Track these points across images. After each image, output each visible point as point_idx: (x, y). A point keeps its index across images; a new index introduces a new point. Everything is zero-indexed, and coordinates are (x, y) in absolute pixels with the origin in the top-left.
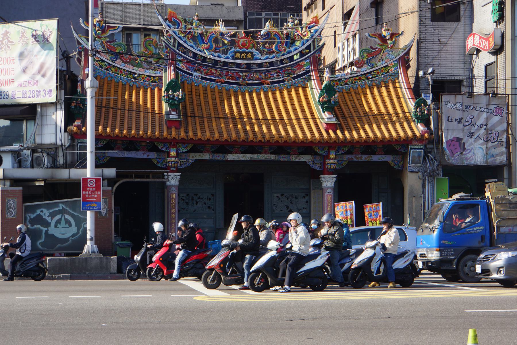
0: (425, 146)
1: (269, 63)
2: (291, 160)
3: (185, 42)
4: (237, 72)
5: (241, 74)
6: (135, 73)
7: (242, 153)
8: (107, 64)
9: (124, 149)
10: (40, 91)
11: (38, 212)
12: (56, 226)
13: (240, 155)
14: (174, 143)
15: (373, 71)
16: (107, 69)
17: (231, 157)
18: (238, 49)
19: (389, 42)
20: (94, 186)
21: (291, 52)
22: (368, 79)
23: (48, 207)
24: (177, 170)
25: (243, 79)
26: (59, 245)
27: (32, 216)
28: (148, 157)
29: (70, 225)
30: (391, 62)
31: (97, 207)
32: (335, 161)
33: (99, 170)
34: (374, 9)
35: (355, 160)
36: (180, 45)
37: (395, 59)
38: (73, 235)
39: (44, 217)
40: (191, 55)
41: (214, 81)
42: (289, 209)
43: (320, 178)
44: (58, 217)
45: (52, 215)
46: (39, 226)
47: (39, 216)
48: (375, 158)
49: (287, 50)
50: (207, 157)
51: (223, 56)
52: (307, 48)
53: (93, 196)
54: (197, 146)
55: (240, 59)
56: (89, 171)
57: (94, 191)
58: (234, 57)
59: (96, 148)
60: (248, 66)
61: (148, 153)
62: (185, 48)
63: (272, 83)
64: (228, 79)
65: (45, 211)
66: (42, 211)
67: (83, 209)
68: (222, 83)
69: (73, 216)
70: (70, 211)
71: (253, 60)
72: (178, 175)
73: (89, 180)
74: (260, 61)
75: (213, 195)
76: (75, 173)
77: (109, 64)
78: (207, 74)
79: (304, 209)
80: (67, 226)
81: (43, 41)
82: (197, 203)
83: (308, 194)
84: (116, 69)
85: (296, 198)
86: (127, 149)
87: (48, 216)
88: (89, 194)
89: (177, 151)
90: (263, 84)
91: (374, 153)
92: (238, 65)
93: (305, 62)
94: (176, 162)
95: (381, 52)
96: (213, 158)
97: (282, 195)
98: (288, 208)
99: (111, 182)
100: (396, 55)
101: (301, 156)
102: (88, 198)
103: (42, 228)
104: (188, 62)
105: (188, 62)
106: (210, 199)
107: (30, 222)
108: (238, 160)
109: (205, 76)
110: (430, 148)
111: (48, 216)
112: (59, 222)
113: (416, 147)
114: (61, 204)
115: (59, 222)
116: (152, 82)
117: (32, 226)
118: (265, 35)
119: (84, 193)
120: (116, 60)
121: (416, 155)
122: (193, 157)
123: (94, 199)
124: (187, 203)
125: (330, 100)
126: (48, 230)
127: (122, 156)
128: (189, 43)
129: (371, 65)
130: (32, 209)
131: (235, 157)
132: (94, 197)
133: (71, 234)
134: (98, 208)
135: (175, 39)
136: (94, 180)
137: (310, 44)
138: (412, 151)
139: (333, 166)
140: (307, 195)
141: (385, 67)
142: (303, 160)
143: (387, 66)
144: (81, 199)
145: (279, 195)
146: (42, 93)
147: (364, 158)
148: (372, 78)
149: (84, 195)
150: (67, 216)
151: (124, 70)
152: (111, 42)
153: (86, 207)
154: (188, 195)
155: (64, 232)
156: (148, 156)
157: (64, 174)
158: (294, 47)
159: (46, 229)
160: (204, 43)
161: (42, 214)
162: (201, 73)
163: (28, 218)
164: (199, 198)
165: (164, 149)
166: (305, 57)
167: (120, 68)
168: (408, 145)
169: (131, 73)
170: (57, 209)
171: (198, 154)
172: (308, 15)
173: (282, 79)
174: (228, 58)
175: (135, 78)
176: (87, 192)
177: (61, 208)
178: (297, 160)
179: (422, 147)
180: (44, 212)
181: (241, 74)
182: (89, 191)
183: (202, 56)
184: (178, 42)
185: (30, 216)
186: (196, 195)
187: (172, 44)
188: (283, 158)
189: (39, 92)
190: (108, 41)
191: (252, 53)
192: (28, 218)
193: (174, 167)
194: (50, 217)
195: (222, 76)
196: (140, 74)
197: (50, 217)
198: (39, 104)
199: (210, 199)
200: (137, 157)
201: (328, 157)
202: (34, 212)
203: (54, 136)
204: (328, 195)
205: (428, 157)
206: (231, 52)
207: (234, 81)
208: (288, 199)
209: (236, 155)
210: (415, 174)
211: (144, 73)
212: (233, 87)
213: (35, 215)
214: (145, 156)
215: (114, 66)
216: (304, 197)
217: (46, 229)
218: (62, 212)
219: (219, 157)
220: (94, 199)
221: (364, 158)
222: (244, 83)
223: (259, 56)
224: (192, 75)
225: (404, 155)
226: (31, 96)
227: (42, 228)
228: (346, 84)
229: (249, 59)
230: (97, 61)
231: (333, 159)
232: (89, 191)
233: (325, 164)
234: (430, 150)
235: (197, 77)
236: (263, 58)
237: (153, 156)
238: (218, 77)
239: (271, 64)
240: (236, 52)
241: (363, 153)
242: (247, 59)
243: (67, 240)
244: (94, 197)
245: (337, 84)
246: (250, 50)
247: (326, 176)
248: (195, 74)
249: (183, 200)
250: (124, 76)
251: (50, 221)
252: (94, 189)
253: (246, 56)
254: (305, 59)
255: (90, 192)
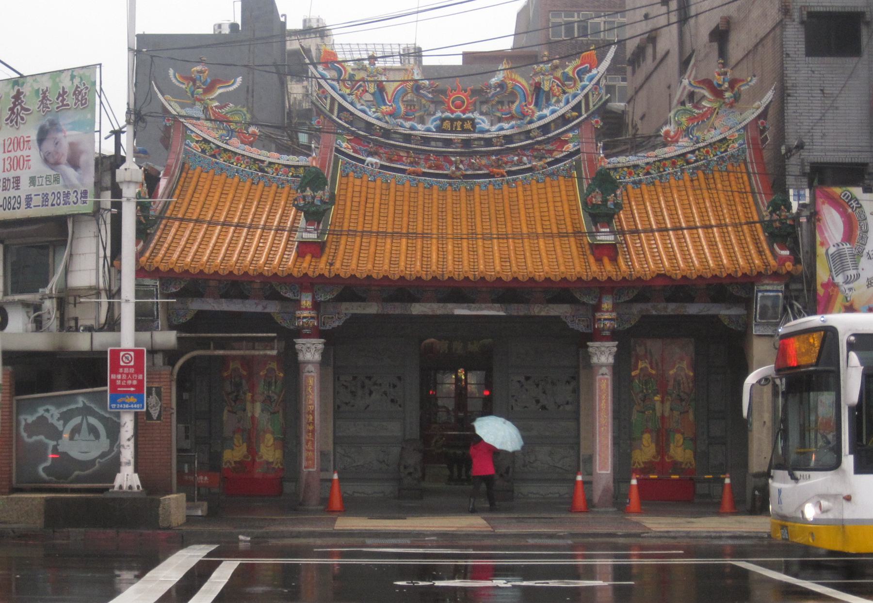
0: (787, 286)
1: (505, 136)
2: (532, 314)
3: (352, 104)
4: (445, 156)
5: (453, 159)
6: (263, 162)
7: (439, 301)
8: (213, 146)
9: (222, 297)
10: (68, 193)
11: (41, 411)
12: (72, 438)
13: (435, 306)
14: (307, 283)
15: (699, 149)
16: (214, 156)
17: (417, 309)
18: (447, 114)
19: (728, 95)
20: (132, 364)
21: (545, 117)
22: (688, 163)
23: (58, 402)
24: (318, 333)
25: (458, 168)
26: (76, 473)
27: (31, 419)
28: (266, 311)
29: (97, 436)
30: (731, 132)
31: (137, 403)
32: (614, 315)
33: (146, 336)
34: (715, 45)
35: (654, 313)
36: (342, 109)
37: (739, 127)
38: (103, 455)
39: (50, 421)
40: (363, 125)
41: (403, 171)
42: (540, 405)
43: (588, 347)
44: (76, 420)
45: (66, 417)
46: (42, 437)
47: (42, 419)
48: (693, 309)
49: (538, 114)
50: (372, 309)
51: (419, 126)
52: (574, 109)
53: (129, 382)
54: (351, 289)
55: (452, 131)
56: (128, 337)
57: (132, 374)
58: (440, 129)
59: (137, 292)
60: (466, 143)
61: (265, 303)
62: (352, 114)
63: (510, 173)
64: (430, 168)
65: (52, 409)
66: (47, 411)
67: (111, 408)
68: (418, 175)
69: (101, 419)
70: (96, 409)
71: (474, 132)
72: (318, 344)
73: (122, 354)
74: (487, 136)
75: (399, 378)
76: (102, 340)
77: (218, 147)
78: (391, 160)
79: (567, 403)
80: (92, 437)
81: (75, 104)
82: (371, 393)
83: (575, 378)
84: (230, 154)
85: (553, 383)
86: (226, 296)
87: (59, 419)
88: (122, 380)
89: (313, 297)
90: (493, 176)
91: (691, 299)
92: (448, 143)
93: (571, 135)
94: (312, 318)
95: (712, 114)
96: (385, 312)
97: (527, 378)
98: (538, 402)
99: (171, 356)
100: (740, 118)
101: (551, 305)
102: (121, 386)
103: (47, 441)
104: (357, 138)
105: (357, 138)
106: (395, 386)
107: (26, 430)
108: (430, 313)
109: (388, 164)
110: (796, 290)
111: (59, 419)
112: (76, 431)
113: (769, 288)
114: (81, 398)
115: (76, 431)
116: (292, 176)
117: (30, 436)
118: (496, 88)
119: (114, 377)
120: (230, 138)
121: (769, 303)
122: (347, 309)
123: (132, 389)
124: (353, 393)
125: (607, 201)
126: (58, 445)
127: (218, 309)
128: (359, 107)
129: (695, 139)
130: (32, 407)
131: (425, 309)
132: (132, 386)
133: (98, 453)
134: (138, 406)
135: (333, 99)
136: (132, 354)
137: (580, 102)
138: (760, 294)
139: (608, 324)
140: (573, 378)
141: (721, 141)
142: (552, 313)
143: (725, 139)
144: (108, 388)
145: (522, 379)
146: (72, 198)
147: (672, 309)
148: (696, 161)
149: (113, 382)
150: (92, 420)
151: (243, 155)
152: (221, 108)
153: (116, 403)
154: (355, 378)
155: (84, 449)
156: (265, 308)
157: (82, 342)
158: (551, 108)
159: (54, 443)
160: (385, 104)
161: (47, 415)
162: (381, 159)
163: (23, 423)
164: (375, 384)
165: (289, 295)
166: (571, 125)
167: (236, 153)
168: (753, 284)
169: (256, 160)
170: (73, 406)
171: (355, 304)
172: (634, 72)
173: (528, 166)
174: (429, 130)
175: (262, 170)
176: (119, 376)
177: (80, 405)
178: (543, 314)
179: (779, 288)
180: (51, 412)
181: (453, 159)
182: (121, 374)
183: (381, 128)
184: (340, 104)
185: (26, 420)
186: (370, 378)
187: (328, 108)
188: (518, 310)
189: (67, 195)
190: (216, 107)
191: (472, 120)
192: (23, 423)
193: (308, 328)
194: (61, 422)
195: (418, 163)
196: (270, 163)
197: (61, 422)
198: (70, 215)
199: (395, 386)
200: (244, 310)
201: (597, 308)
202: (34, 411)
203: (94, 273)
204: (600, 380)
205: (792, 306)
206: (435, 120)
207: (441, 172)
208: (537, 385)
209: (428, 305)
210: (767, 340)
211: (277, 161)
212: (439, 182)
213: (34, 418)
214: (259, 309)
215: (226, 150)
216: (568, 382)
217: (54, 443)
218: (86, 411)
219: (396, 309)
220: (132, 389)
221: (672, 309)
222: (459, 173)
223: (486, 125)
224: (363, 161)
225: (748, 302)
226: (55, 202)
227: (47, 441)
228: (648, 173)
229: (467, 131)
230: (197, 142)
231: (607, 311)
232: (123, 373)
233: (595, 320)
234: (796, 293)
235: (372, 165)
236: (494, 128)
237: (273, 308)
238: (411, 164)
239: (509, 139)
240: (443, 120)
241: (669, 300)
242: (464, 131)
243: (92, 462)
244: (132, 386)
245: (630, 174)
246: (470, 115)
247: (597, 344)
248: (369, 159)
249: (346, 387)
250: (243, 166)
251: (60, 428)
252: (132, 370)
253: (462, 126)
254: (571, 129)
255: (124, 376)
